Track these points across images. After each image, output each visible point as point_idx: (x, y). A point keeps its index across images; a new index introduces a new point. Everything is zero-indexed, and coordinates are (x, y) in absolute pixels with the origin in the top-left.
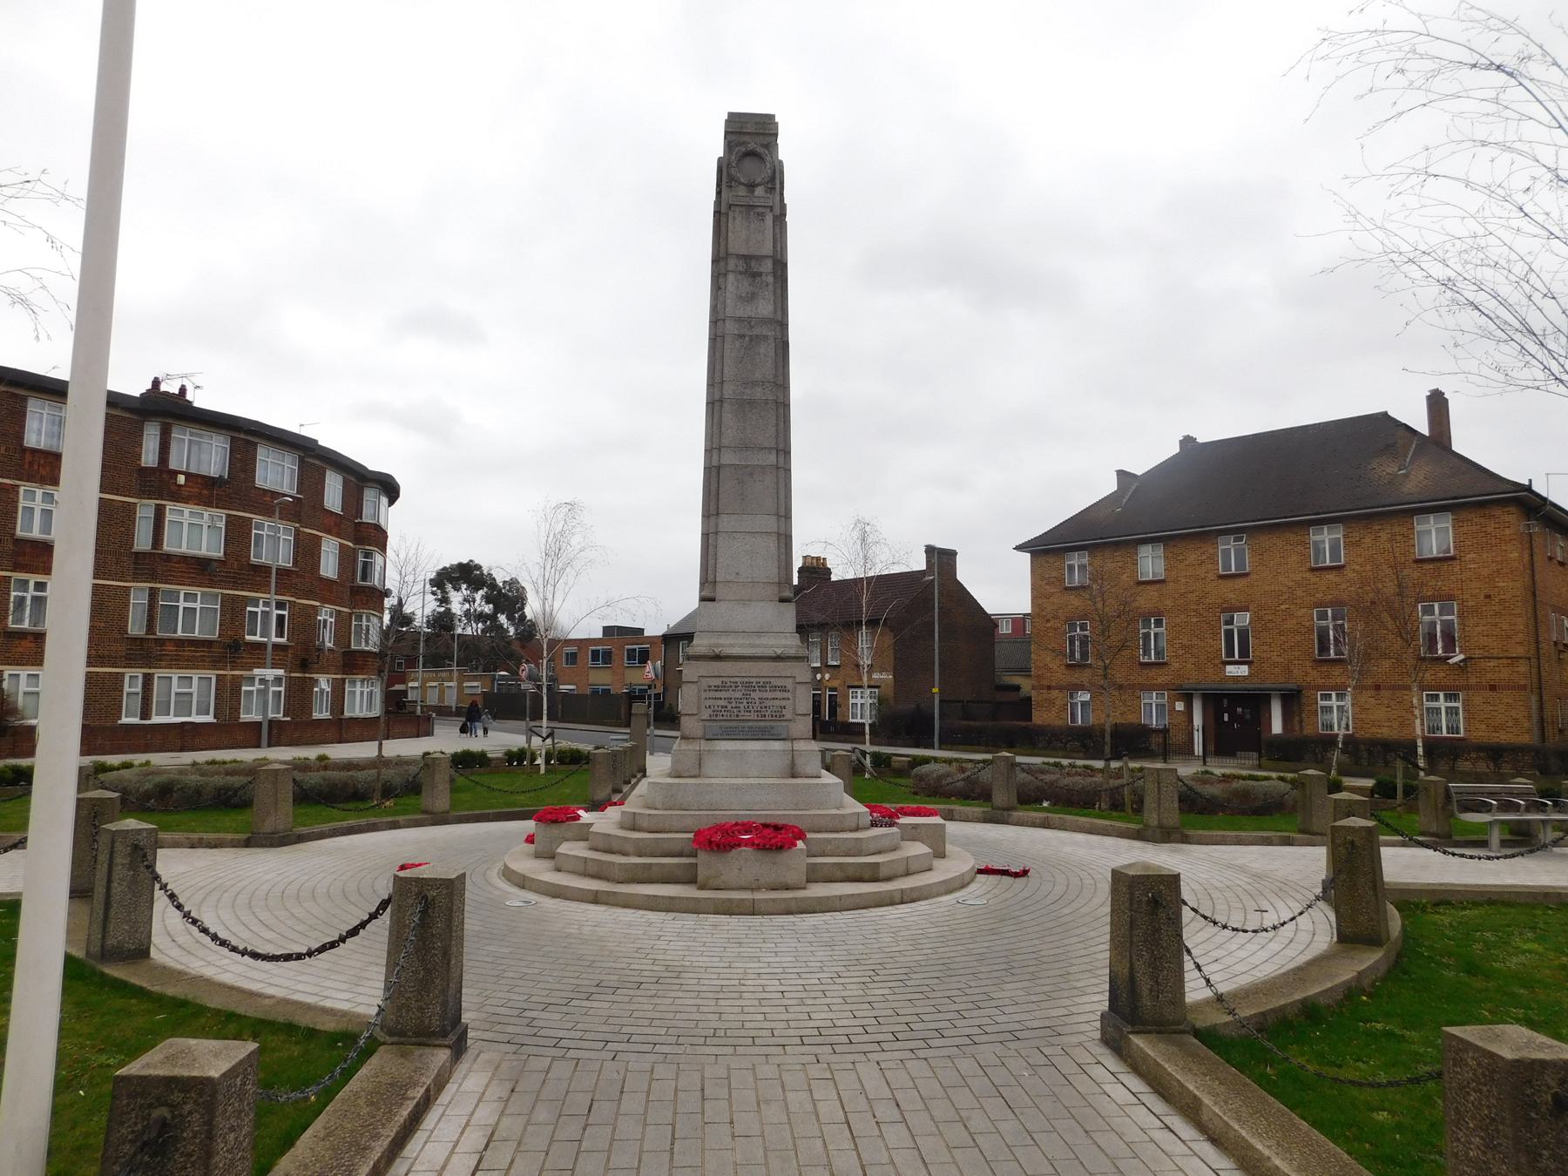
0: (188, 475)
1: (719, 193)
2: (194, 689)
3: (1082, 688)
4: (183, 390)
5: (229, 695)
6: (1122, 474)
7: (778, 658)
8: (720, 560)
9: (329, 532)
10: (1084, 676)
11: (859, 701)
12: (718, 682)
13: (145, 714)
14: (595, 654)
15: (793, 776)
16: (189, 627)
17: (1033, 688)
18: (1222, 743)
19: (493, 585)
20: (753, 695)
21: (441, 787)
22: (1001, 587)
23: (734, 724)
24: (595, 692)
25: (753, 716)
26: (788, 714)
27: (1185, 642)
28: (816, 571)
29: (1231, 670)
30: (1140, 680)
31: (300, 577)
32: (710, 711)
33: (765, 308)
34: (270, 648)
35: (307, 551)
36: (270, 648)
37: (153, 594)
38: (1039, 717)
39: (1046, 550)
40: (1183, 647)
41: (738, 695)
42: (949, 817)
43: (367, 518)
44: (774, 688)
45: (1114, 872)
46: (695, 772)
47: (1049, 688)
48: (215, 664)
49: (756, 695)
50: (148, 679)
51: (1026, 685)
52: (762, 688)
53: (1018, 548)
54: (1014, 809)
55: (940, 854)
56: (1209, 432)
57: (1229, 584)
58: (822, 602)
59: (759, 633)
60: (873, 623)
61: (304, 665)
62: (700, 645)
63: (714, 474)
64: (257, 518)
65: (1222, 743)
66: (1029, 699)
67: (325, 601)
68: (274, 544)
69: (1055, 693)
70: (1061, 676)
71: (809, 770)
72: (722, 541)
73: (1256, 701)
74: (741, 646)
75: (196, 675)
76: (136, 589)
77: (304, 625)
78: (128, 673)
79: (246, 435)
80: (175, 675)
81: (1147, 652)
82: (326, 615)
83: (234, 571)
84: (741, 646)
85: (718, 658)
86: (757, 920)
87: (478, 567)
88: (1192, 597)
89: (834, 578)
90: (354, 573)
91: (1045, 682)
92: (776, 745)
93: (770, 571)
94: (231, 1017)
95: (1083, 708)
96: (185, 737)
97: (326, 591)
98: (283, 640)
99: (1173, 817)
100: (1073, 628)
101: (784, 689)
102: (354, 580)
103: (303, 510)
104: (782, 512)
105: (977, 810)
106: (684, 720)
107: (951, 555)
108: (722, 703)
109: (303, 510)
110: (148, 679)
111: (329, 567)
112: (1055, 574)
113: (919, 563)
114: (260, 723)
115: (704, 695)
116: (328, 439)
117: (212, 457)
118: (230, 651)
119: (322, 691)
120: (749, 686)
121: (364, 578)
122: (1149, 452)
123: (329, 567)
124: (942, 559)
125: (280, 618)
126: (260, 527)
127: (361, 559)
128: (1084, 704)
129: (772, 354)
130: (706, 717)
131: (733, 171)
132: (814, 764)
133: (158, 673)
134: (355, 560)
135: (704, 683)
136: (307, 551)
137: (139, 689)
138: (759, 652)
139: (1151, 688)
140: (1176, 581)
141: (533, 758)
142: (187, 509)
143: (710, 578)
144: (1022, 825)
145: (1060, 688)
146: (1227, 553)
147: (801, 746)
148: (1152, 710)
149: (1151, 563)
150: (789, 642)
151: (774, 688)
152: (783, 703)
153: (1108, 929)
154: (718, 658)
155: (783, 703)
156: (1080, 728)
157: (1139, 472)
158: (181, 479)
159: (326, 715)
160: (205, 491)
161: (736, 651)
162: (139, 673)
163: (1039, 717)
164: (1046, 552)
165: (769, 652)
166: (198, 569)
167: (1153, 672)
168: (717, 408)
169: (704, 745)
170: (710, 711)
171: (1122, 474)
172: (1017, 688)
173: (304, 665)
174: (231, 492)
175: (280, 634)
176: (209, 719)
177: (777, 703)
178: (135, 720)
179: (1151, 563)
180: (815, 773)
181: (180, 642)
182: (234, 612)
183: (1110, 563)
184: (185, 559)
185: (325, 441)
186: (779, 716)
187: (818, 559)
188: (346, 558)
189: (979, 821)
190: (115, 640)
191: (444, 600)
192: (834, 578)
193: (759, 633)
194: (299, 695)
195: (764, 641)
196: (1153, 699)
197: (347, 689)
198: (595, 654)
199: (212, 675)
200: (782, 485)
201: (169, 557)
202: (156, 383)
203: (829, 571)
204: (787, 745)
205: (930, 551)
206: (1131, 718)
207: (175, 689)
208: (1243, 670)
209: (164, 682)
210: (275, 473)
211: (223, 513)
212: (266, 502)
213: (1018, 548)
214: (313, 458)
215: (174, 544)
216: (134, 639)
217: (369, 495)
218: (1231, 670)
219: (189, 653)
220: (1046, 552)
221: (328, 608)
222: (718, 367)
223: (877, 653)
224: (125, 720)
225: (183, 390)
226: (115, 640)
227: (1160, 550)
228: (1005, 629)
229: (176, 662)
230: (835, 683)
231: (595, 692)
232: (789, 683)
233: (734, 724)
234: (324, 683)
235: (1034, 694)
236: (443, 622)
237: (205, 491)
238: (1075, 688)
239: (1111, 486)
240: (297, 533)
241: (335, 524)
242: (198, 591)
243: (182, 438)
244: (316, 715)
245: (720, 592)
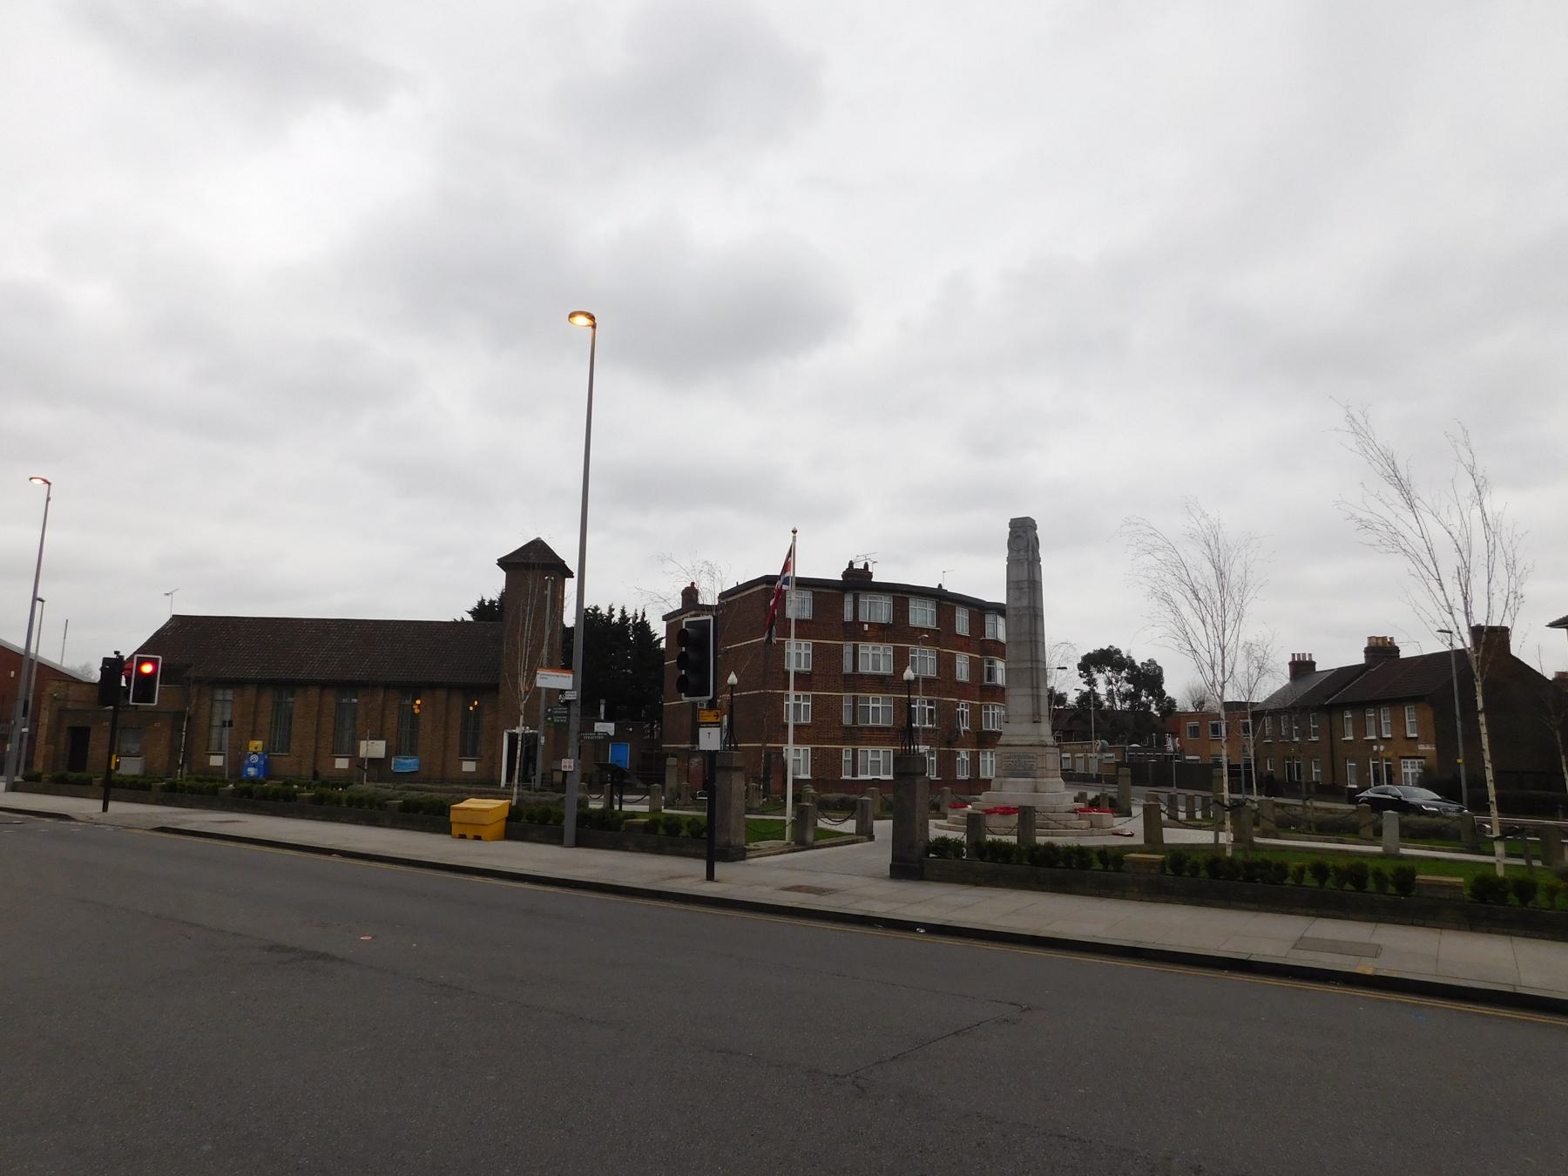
4: (866, 565)
11: (1410, 771)
13: (855, 774)
16: (876, 719)
19: (1130, 664)
31: (944, 682)
35: (946, 664)
37: (855, 699)
48: (892, 742)
50: (855, 752)
61: (949, 744)
64: (912, 647)
75: (881, 749)
77: (947, 716)
78: (845, 748)
79: (902, 594)
80: (870, 749)
82: (964, 708)
87: (1118, 652)
89: (1403, 655)
97: (962, 690)
99: (1272, 826)
103: (942, 636)
109: (942, 636)
110: (855, 752)
111: (962, 671)
113: (1464, 641)
117: (879, 611)
123: (962, 671)
126: (914, 652)
133: (860, 748)
136: (946, 664)
142: (870, 645)
159: (966, 777)
160: (881, 632)
166: (879, 683)
174: (897, 632)
176: (890, 777)
181: (872, 729)
184: (871, 676)
185: (951, 587)
186: (1031, 768)
188: (975, 667)
191: (1091, 682)
192: (1403, 655)
201: (862, 676)
202: (851, 564)
203: (1397, 650)
210: (922, 615)
211: (890, 646)
212: (915, 635)
214: (943, 600)
215: (866, 667)
216: (846, 728)
217: (989, 619)
219: (876, 736)
221: (964, 702)
223: (1420, 726)
225: (866, 565)
229: (869, 742)
230: (1390, 754)
234: (964, 755)
236: (1087, 698)
237: (881, 632)
240: (938, 654)
241: (964, 644)
243: (865, 600)
244: (959, 777)
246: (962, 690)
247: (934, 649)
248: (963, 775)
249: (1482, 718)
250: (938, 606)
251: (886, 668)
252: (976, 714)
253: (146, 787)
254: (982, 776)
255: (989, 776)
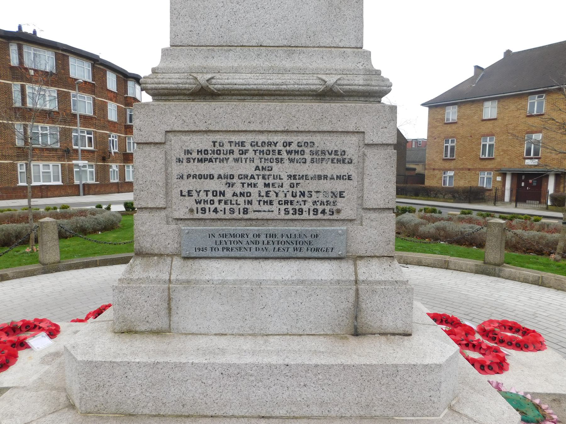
0: (35, 71)
2: (51, 170)
3: (450, 170)
4: (20, 27)
5: (68, 172)
9: (111, 100)
10: (452, 164)
18: (520, 197)
20: (277, 169)
23: (239, 228)
25: (276, 211)
26: (347, 207)
27: (505, 148)
29: (528, 162)
30: (480, 166)
31: (97, 120)
32: (190, 202)
34: (80, 151)
35: (100, 109)
36: (80, 151)
38: (428, 183)
39: (436, 106)
40: (503, 151)
41: (248, 169)
43: (130, 94)
44: (320, 156)
46: (160, 323)
47: (434, 169)
48: (59, 159)
49: (282, 170)
52: (296, 154)
53: (423, 105)
56: (519, 45)
57: (530, 119)
59: (290, 48)
61: (104, 159)
64: (72, 92)
65: (520, 197)
67: (112, 131)
68: (83, 104)
69: (436, 172)
70: (440, 164)
73: (540, 177)
74: (253, 71)
75: (51, 164)
76: (17, 124)
78: (19, 163)
79: (63, 52)
80: (41, 164)
81: (484, 153)
83: (64, 116)
84: (253, 71)
88: (510, 127)
90: (126, 119)
91: (432, 167)
92: (323, 270)
95: (449, 179)
96: (44, 191)
97: (112, 126)
98: (92, 148)
100: (447, 142)
101: (340, 158)
102: (126, 122)
105: (471, 263)
109: (95, 87)
112: (440, 117)
114: (79, 185)
115: (176, 169)
116: (105, 56)
117: (46, 61)
118: (66, 153)
119: (114, 171)
120: (268, 152)
121: (131, 121)
122: (490, 57)
123: (112, 115)
125: (90, 139)
127: (128, 113)
128: (450, 177)
130: (182, 213)
134: (126, 113)
135: (177, 145)
136: (100, 109)
137: (24, 170)
138: (290, 81)
139: (484, 170)
140: (503, 119)
145: (439, 170)
146: (532, 105)
148: (484, 180)
149: (490, 110)
151: (320, 156)
152: (339, 186)
155: (339, 186)
158: (32, 73)
159: (116, 181)
161: (240, 80)
162: (24, 162)
163: (428, 183)
164: (436, 106)
165: (312, 82)
166: (46, 116)
167: (487, 162)
169: (179, 270)
171: (477, 68)
172: (415, 169)
173: (104, 159)
174: (60, 78)
175: (90, 145)
176: (60, 183)
177: (326, 185)
178: (25, 184)
179: (490, 110)
182: (65, 135)
183: (468, 110)
185: (104, 56)
186: (328, 210)
188: (121, 113)
189: (471, 271)
190: (11, 148)
193: (290, 48)
194: (102, 173)
195: (300, 61)
196: (486, 175)
197: (126, 170)
199: (59, 163)
206: (473, 184)
207: (42, 170)
208: (535, 162)
209: (36, 167)
210: (80, 71)
213: (423, 105)
214: (99, 66)
216: (19, 148)
218: (528, 162)
219: (46, 153)
220: (436, 106)
221: (113, 134)
224: (20, 184)
226: (11, 148)
227: (496, 103)
232: (350, 145)
233: (239, 228)
234: (114, 167)
237: (47, 79)
238: (445, 170)
239: (471, 73)
241: (114, 97)
242: (47, 126)
243: (29, 52)
244: (112, 181)
246: (112, 126)
247: (91, 97)
248: (114, 179)
249: (5, 122)
250: (93, 67)
251: (51, 105)
252: (122, 143)
253: (150, 91)
254: (127, 180)
255: (131, 180)
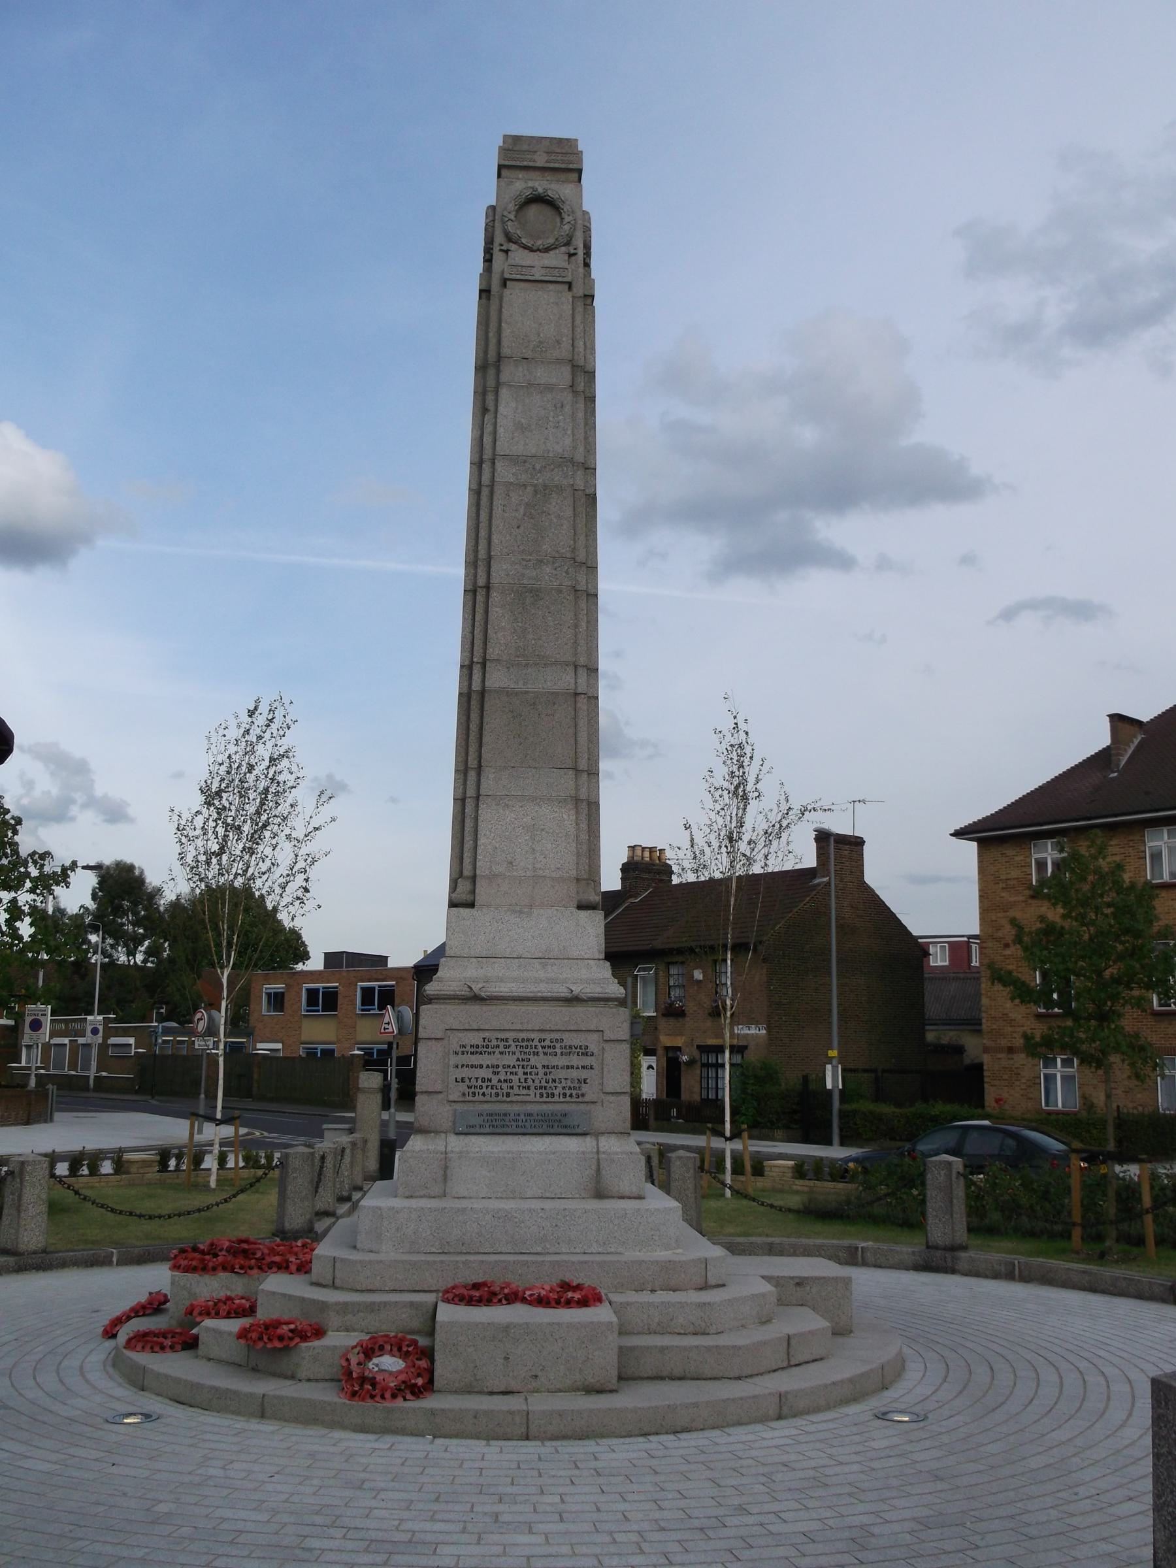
1: (488, 260)
6: (1117, 720)
7: (573, 1000)
8: (482, 841)
12: (476, 1039)
14: (312, 994)
15: (600, 1194)
17: (986, 1050)
20: (534, 1060)
21: (32, 1211)
22: (934, 893)
24: (311, 1054)
28: (645, 869)
32: (463, 1087)
33: (562, 443)
41: (510, 1060)
42: (853, 1258)
44: (569, 1050)
45: (1156, 1383)
51: (973, 1046)
52: (549, 1050)
54: (964, 1248)
55: (840, 1331)
58: (653, 920)
60: (740, 948)
62: (448, 979)
63: (474, 703)
66: (979, 1068)
71: (625, 1186)
72: (487, 813)
85: (476, 998)
86: (530, 1449)
91: (1004, 1042)
93: (558, 856)
94: (632, 1073)
101: (585, 1052)
104: (583, 764)
106: (419, 1099)
107: (854, 844)
108: (485, 1073)
112: (1015, 873)
115: (454, 1060)
120: (526, 1046)
124: (840, 849)
129: (569, 513)
131: (511, 227)
132: (632, 1176)
135: (455, 1040)
138: (543, 989)
141: (198, 1160)
143: (467, 872)
144: (977, 1274)
147: (611, 1145)
150: (600, 978)
151: (569, 1050)
152: (583, 1074)
153: (1148, 1485)
154: (476, 998)
155: (583, 1074)
156: (1058, 1113)
157: (1145, 717)
161: (504, 989)
168: (480, 598)
169: (455, 1143)
170: (463, 1087)
171: (1117, 720)
177: (574, 1074)
180: (635, 1190)
186: (575, 1092)
187: (652, 850)
198: (312, 994)
200: (582, 723)
203: (669, 871)
204: (588, 1143)
205: (823, 837)
213: (959, 834)
222: (483, 533)
228: (938, 959)
231: (311, 1054)
232: (592, 1042)
235: (986, 1059)
245: (483, 892)
